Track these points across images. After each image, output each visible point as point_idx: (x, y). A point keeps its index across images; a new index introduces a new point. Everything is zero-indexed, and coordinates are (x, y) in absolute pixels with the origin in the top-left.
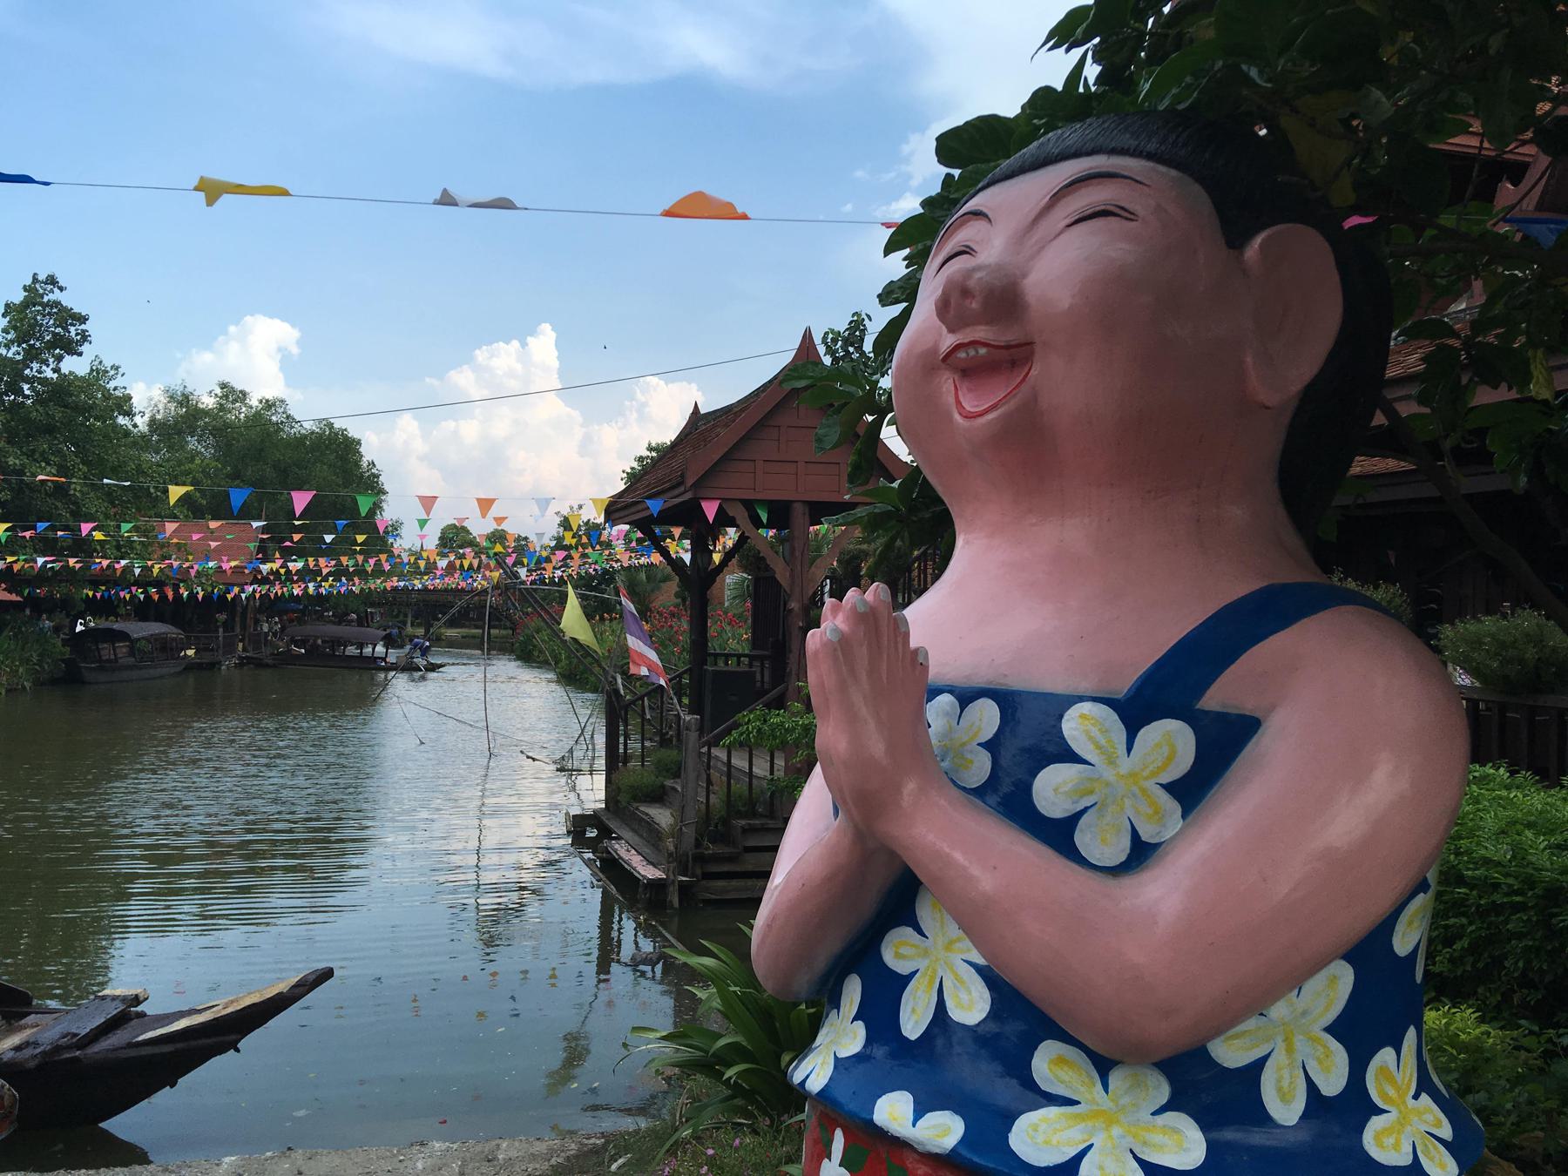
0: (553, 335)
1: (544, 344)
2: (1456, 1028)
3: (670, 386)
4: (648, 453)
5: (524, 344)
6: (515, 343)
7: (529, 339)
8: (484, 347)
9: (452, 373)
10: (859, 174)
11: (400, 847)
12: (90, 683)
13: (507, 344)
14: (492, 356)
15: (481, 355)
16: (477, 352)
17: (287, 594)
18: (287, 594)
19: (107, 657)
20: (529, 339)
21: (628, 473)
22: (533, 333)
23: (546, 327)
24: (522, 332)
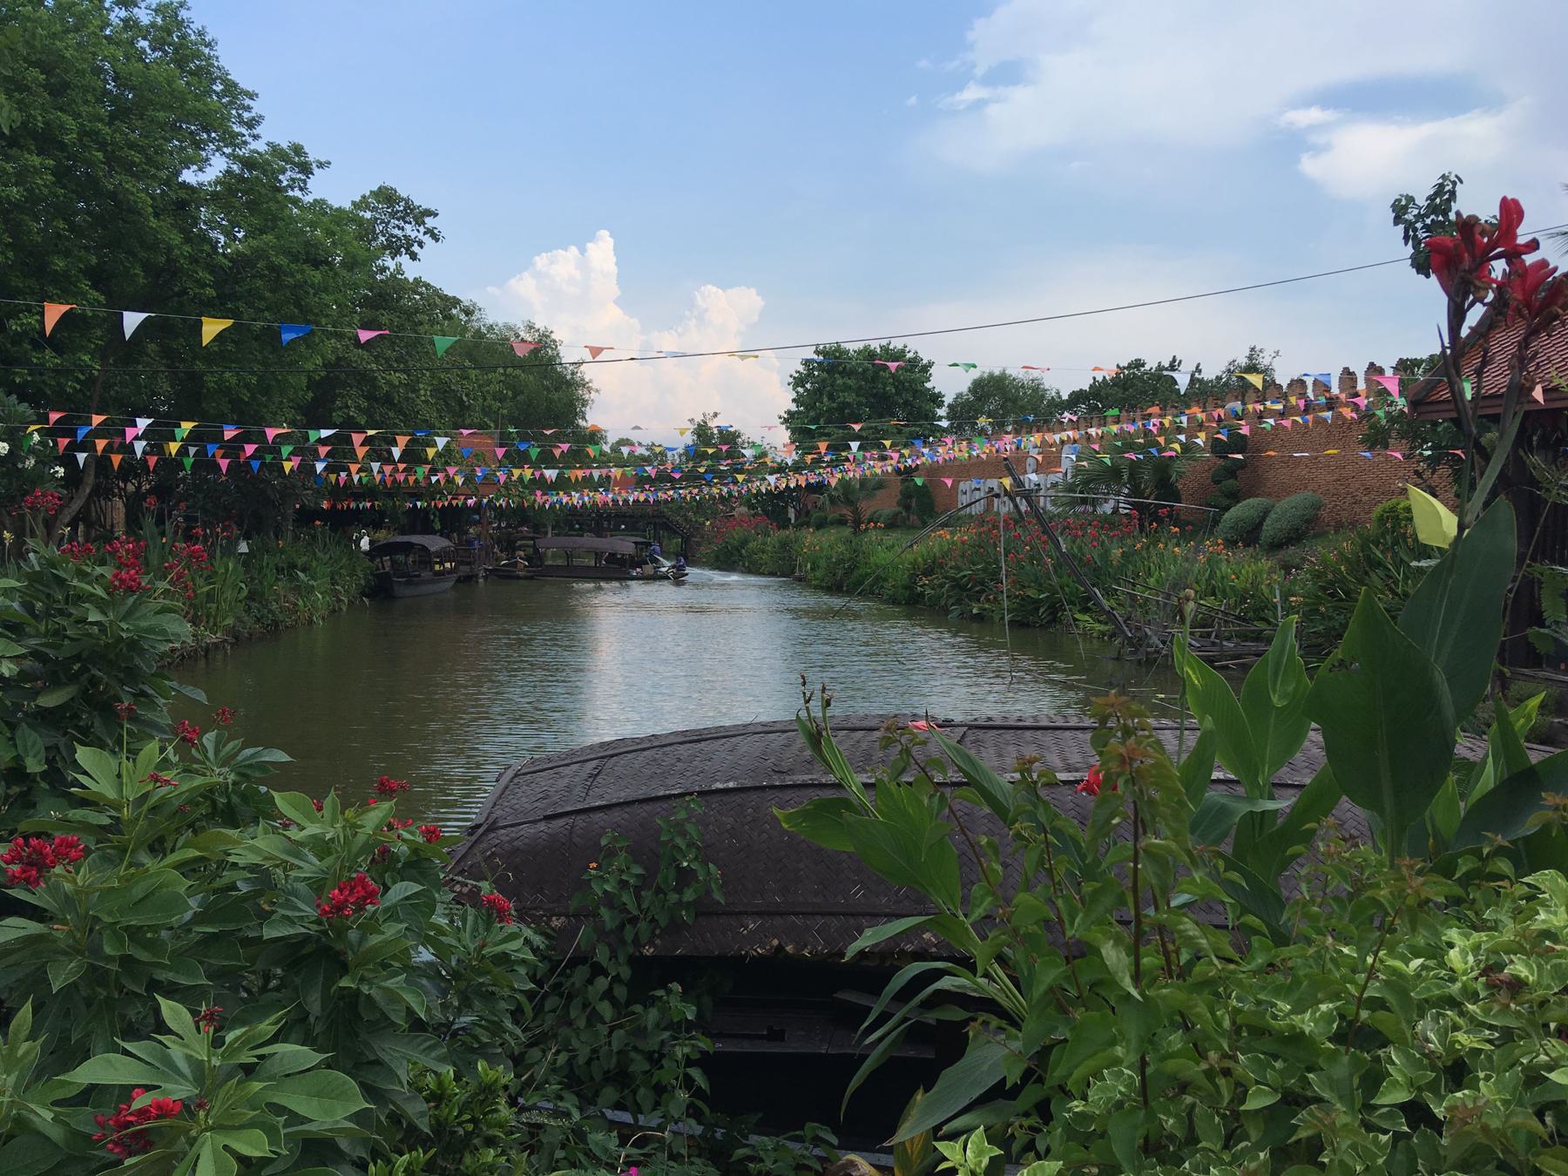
0: (611, 241)
1: (603, 251)
2: (266, 575)
3: (729, 291)
4: (815, 357)
5: (583, 251)
6: (574, 250)
7: (589, 245)
8: (544, 254)
9: (513, 282)
10: (923, 64)
11: (491, 716)
12: (400, 598)
13: (566, 250)
14: (552, 263)
15: (541, 261)
16: (537, 258)
17: (389, 481)
18: (389, 481)
19: (385, 558)
20: (589, 245)
21: (795, 378)
22: (592, 238)
23: (604, 233)
24: (582, 240)
